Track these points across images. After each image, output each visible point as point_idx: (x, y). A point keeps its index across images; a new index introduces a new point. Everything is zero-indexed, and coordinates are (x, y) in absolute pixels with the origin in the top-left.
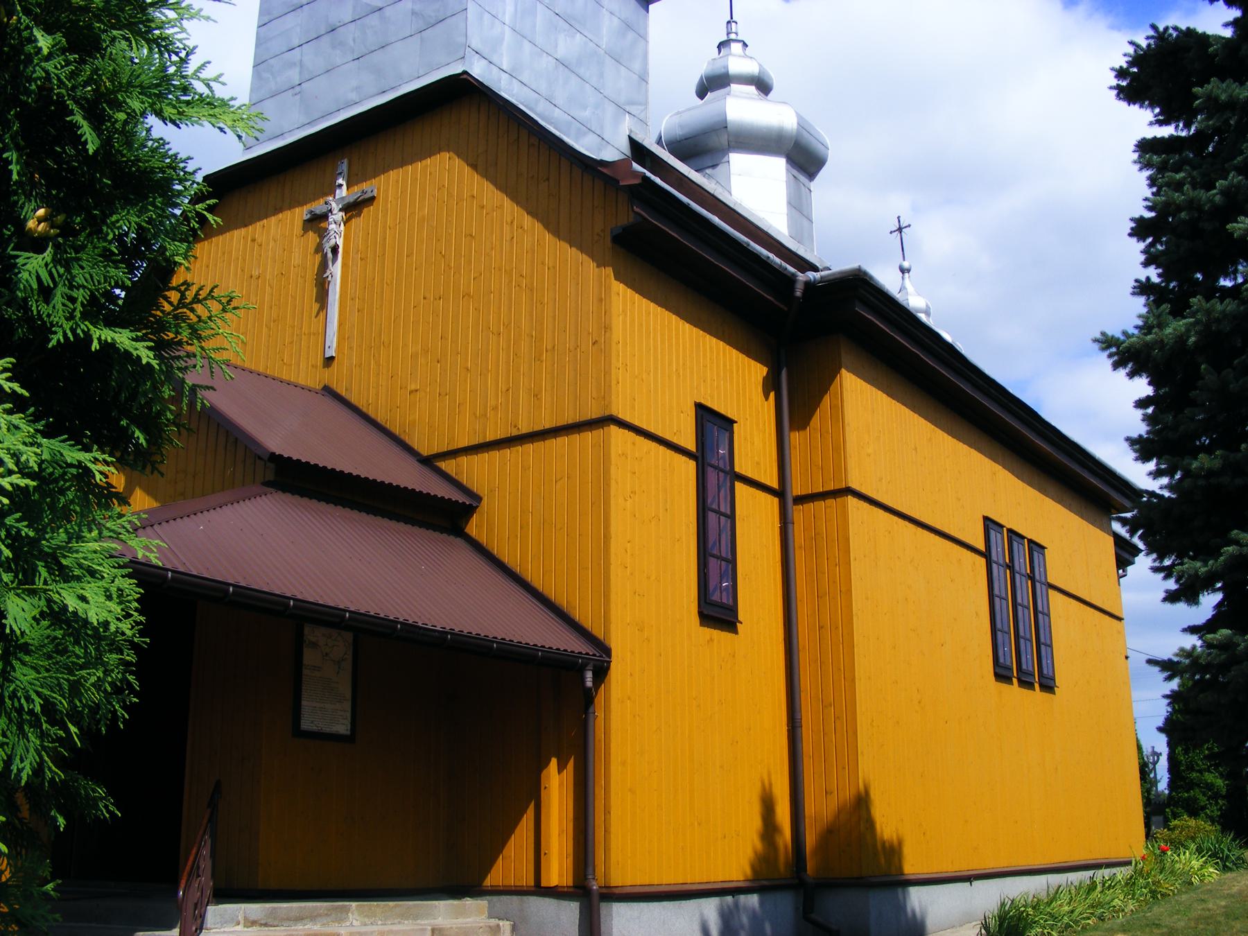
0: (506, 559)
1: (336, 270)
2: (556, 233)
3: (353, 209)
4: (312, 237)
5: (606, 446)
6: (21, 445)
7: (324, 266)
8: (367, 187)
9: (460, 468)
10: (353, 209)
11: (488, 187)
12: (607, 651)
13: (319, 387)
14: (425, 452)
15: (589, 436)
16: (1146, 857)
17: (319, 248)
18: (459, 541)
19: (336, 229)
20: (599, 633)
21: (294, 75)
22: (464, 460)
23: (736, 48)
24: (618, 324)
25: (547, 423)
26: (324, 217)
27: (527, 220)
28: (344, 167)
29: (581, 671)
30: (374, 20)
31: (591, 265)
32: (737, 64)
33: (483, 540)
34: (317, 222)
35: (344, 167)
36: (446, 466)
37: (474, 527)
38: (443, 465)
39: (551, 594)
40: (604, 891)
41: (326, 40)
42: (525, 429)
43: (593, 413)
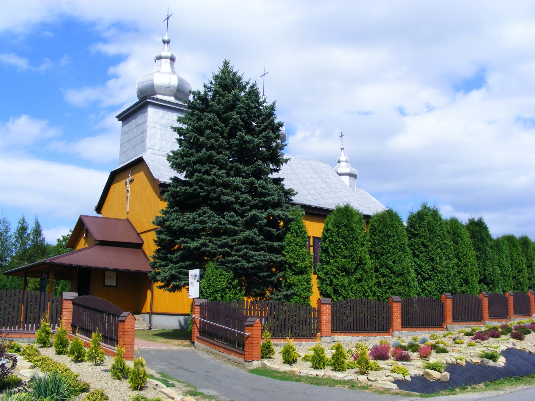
31: (157, 198)
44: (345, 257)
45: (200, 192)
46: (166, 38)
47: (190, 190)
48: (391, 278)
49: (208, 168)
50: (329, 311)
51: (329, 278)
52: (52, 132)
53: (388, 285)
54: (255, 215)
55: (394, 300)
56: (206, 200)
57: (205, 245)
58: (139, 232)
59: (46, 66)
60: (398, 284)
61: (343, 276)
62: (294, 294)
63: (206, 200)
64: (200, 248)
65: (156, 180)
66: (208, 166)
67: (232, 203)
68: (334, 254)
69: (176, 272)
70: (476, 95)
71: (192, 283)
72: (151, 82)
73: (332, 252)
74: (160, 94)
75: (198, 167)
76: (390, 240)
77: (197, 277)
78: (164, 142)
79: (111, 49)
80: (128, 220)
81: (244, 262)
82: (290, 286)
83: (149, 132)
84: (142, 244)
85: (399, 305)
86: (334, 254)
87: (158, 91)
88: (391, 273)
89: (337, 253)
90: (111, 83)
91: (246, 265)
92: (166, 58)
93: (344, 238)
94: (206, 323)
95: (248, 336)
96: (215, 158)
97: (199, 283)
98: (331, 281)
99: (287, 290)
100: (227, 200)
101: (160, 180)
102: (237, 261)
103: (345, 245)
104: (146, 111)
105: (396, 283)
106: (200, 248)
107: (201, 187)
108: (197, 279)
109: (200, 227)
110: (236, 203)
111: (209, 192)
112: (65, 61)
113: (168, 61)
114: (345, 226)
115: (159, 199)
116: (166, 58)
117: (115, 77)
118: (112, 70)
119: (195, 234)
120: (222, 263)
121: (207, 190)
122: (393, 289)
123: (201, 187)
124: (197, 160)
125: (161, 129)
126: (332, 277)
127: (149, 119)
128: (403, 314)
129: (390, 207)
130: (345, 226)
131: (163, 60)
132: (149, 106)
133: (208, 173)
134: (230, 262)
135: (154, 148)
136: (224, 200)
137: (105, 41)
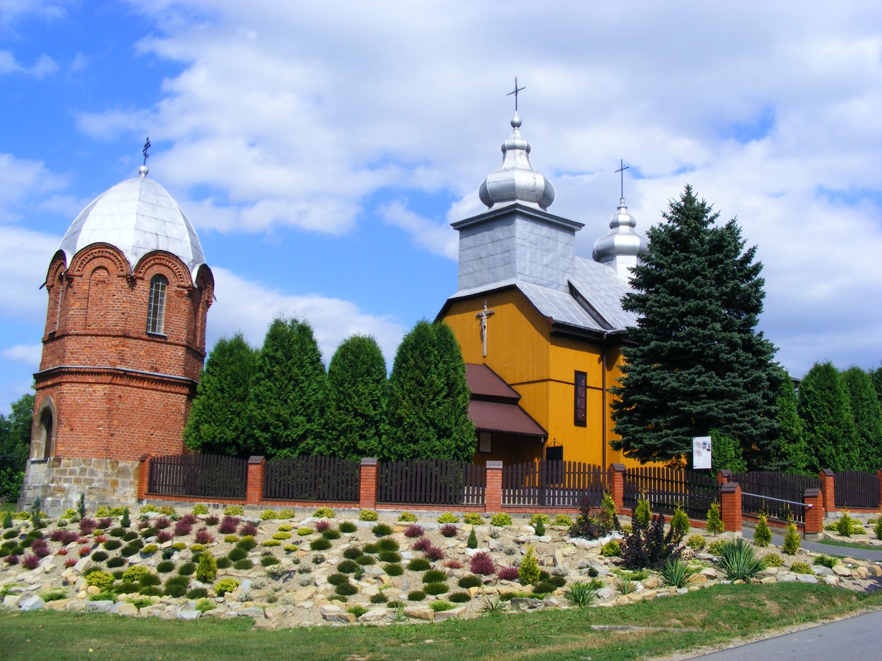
0: (527, 411)
1: (485, 332)
2: (538, 331)
3: (489, 315)
4: (478, 321)
5: (548, 387)
6: (489, 487)
7: (482, 331)
8: (492, 310)
9: (518, 388)
10: (489, 315)
11: (522, 315)
12: (547, 433)
13: (481, 363)
14: (509, 383)
15: (545, 383)
16: (109, 488)
17: (480, 325)
18: (516, 407)
19: (485, 322)
20: (546, 430)
21: (471, 270)
22: (517, 386)
23: (623, 210)
24: (551, 356)
25: (536, 379)
26: (482, 316)
27: (531, 326)
28: (486, 302)
29: (541, 438)
30: (491, 258)
31: (545, 341)
32: (623, 218)
33: (522, 406)
34: (479, 317)
35: (486, 302)
36: (514, 387)
37: (520, 403)
38: (513, 387)
39: (537, 420)
40: (753, 514)
41: (479, 261)
42: (531, 380)
43: (545, 378)
44: (832, 424)
45: (692, 348)
46: (516, 120)
47: (681, 345)
48: (866, 447)
49: (701, 321)
50: (832, 484)
51: (814, 447)
52: (54, 182)
53: (864, 456)
54: (760, 376)
55: (616, 469)
56: (699, 358)
57: (710, 409)
58: (573, 386)
59: (45, 67)
60: (875, 455)
61: (829, 445)
62: (790, 465)
63: (699, 358)
64: (706, 412)
65: (548, 320)
66: (701, 318)
67: (732, 362)
68: (819, 420)
69: (674, 440)
70: (757, 149)
71: (698, 452)
72: (510, 182)
73: (816, 417)
74: (521, 199)
75: (690, 318)
76: (864, 404)
77: (707, 446)
78: (534, 265)
79: (169, 49)
80: (484, 364)
81: (752, 429)
82: (784, 456)
83: (519, 252)
84: (518, 399)
85: (831, 478)
86: (819, 420)
87: (519, 196)
88: (867, 442)
89: (823, 419)
90: (165, 104)
91: (755, 432)
92: (521, 148)
93: (830, 402)
94: (745, 495)
95: (810, 508)
96: (709, 309)
97: (710, 452)
98: (817, 450)
99: (779, 461)
100: (728, 358)
101: (554, 318)
102: (744, 428)
103: (830, 410)
104: (512, 223)
105: (872, 454)
106: (706, 412)
107: (693, 342)
108: (707, 448)
109: (702, 388)
110: (737, 361)
111: (703, 348)
112: (80, 63)
113: (524, 152)
114: (829, 388)
115: (549, 343)
116: (521, 148)
117: (171, 95)
118: (168, 84)
119: (693, 397)
120: (728, 430)
121: (701, 346)
122: (870, 460)
123: (693, 342)
124: (687, 310)
125: (530, 247)
126: (818, 446)
127: (518, 235)
128: (835, 487)
129: (829, 360)
130: (829, 388)
131: (518, 151)
132: (518, 216)
133: (703, 326)
134: (737, 429)
135: (524, 273)
136: (724, 359)
137: (160, 34)
